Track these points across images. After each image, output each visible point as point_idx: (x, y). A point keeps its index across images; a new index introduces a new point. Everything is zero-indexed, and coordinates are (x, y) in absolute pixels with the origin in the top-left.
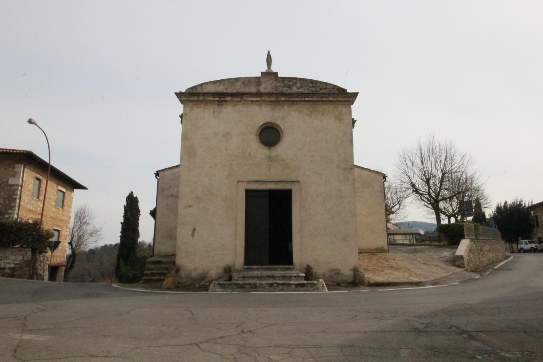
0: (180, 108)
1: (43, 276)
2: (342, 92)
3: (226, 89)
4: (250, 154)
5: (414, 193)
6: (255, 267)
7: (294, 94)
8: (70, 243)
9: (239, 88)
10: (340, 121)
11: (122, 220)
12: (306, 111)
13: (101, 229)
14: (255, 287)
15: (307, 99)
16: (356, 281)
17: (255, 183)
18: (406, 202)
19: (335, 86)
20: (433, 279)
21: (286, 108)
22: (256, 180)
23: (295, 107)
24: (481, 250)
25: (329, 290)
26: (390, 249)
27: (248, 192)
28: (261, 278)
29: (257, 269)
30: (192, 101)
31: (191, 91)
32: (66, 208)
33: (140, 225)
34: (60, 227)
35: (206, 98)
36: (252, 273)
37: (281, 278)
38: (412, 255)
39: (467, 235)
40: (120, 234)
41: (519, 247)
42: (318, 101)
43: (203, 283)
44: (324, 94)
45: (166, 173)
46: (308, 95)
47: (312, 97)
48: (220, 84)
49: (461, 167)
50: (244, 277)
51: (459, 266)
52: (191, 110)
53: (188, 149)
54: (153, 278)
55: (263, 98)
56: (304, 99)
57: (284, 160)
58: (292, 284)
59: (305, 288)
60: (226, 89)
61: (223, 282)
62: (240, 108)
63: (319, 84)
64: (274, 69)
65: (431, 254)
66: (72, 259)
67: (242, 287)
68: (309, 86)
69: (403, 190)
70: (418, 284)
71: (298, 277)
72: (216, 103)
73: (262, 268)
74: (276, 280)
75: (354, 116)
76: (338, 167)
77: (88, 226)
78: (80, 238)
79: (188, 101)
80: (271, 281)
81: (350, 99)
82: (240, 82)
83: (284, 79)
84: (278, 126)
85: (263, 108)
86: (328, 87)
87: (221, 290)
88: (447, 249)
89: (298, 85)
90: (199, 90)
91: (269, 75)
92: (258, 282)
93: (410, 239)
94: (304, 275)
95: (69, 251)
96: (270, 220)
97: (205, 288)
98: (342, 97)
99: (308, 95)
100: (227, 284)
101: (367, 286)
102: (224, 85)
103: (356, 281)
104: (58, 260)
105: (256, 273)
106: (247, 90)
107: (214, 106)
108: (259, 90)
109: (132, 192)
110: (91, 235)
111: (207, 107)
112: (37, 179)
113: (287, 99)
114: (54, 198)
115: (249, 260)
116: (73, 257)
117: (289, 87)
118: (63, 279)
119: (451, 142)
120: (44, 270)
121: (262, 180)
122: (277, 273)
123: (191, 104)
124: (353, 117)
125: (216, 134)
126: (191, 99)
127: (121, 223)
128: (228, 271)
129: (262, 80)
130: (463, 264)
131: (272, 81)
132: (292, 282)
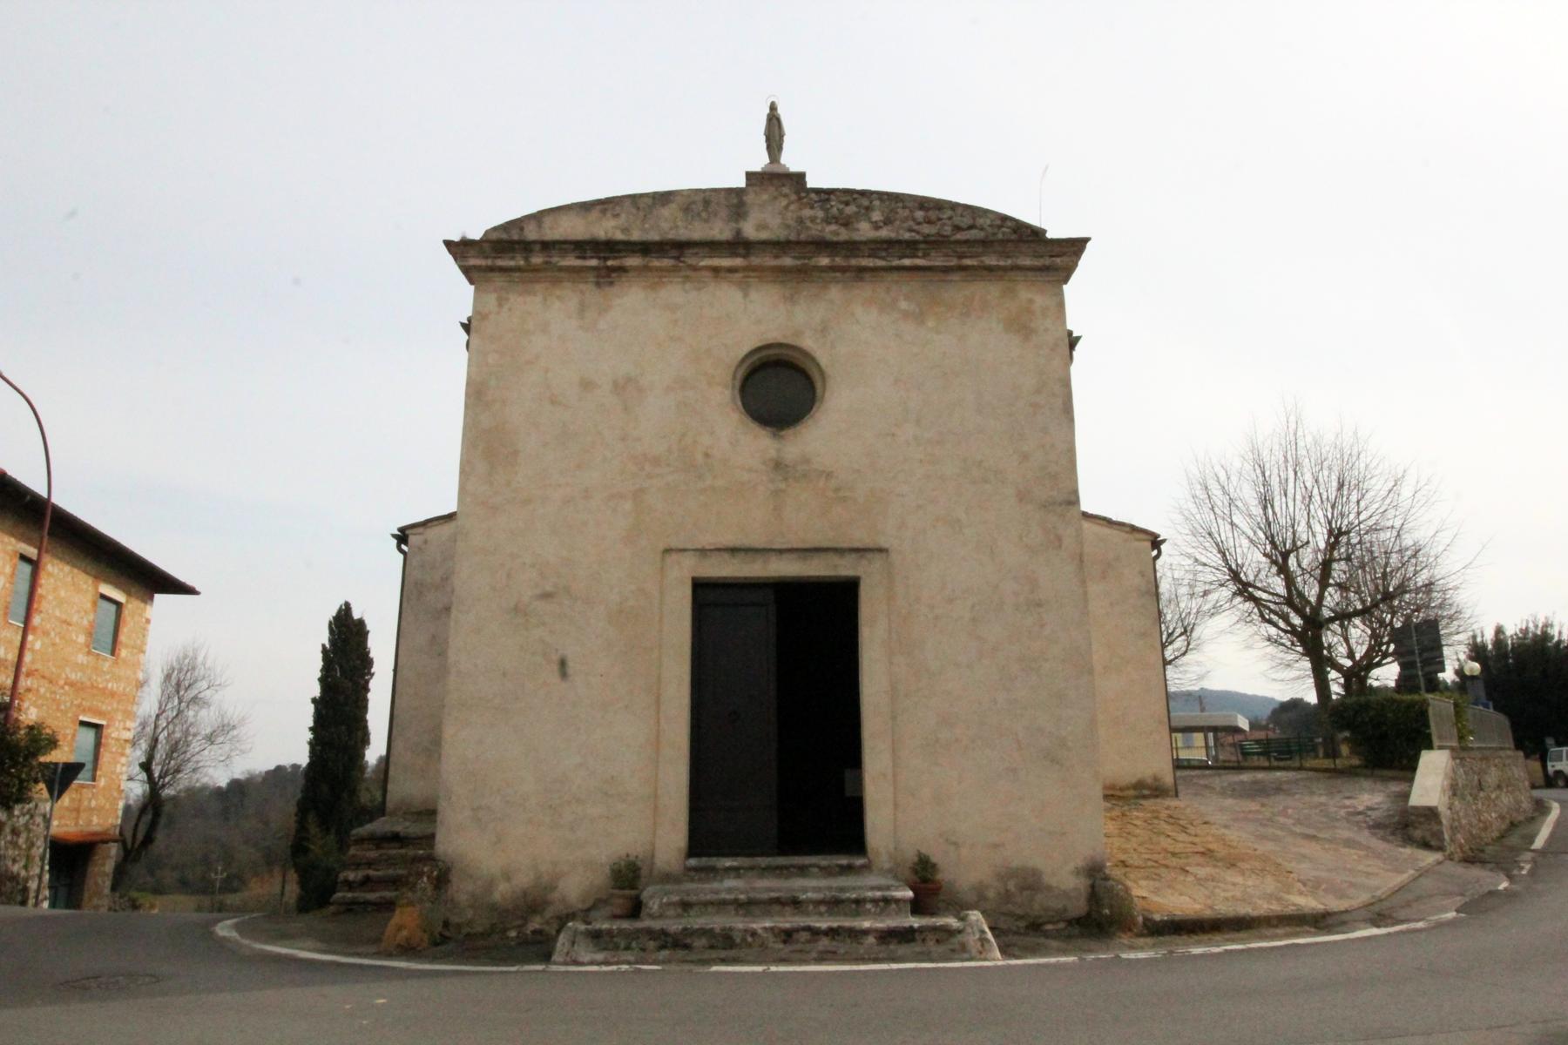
0: (460, 295)
1: (26, 880)
2: (1029, 236)
3: (625, 230)
4: (707, 455)
5: (1239, 599)
6: (728, 862)
7: (861, 242)
8: (146, 767)
9: (669, 225)
10: (1027, 338)
11: (316, 691)
12: (903, 305)
13: (243, 721)
14: (726, 945)
15: (907, 262)
16: (1099, 917)
17: (726, 556)
18: (1206, 630)
19: (1005, 218)
20: (1364, 897)
21: (835, 293)
22: (731, 545)
23: (866, 290)
24: (1481, 787)
25: (1006, 951)
26: (1180, 788)
27: (701, 587)
28: (747, 906)
29: (735, 871)
30: (502, 270)
31: (504, 236)
32: (124, 653)
33: (371, 705)
34: (100, 714)
35: (555, 260)
36: (716, 885)
37: (823, 908)
38: (1253, 806)
39: (1440, 738)
40: (309, 736)
41: (1550, 770)
42: (946, 270)
43: (535, 924)
44: (966, 242)
45: (433, 533)
46: (910, 247)
47: (924, 257)
48: (604, 212)
49: (1391, 513)
50: (686, 906)
51: (1426, 845)
52: (501, 302)
53: (487, 443)
54: (372, 896)
55: (755, 261)
56: (896, 263)
57: (829, 475)
58: (866, 932)
59: (917, 947)
60: (625, 230)
61: (605, 926)
62: (675, 293)
63: (949, 213)
64: (791, 160)
65: (1316, 799)
66: (148, 817)
67: (675, 943)
68: (914, 219)
69: (1199, 589)
70: (1320, 921)
71: (887, 901)
72: (591, 278)
73: (752, 868)
74: (808, 914)
75: (1073, 323)
76: (1022, 497)
77: (203, 713)
78: (174, 748)
79: (491, 269)
80: (788, 921)
81: (1058, 260)
82: (673, 206)
83: (826, 194)
84: (806, 354)
85: (754, 295)
86: (980, 221)
87: (600, 957)
88: (1366, 784)
89: (876, 216)
90: (531, 234)
91: (777, 181)
92: (738, 923)
93: (1207, 747)
94: (910, 894)
95: (137, 789)
96: (781, 686)
97: (540, 948)
98: (1033, 258)
99: (910, 247)
100: (620, 931)
101: (1140, 935)
102: (617, 216)
103: (1099, 917)
104: (95, 820)
105: (731, 886)
106: (697, 231)
107: (582, 286)
108: (738, 232)
109: (347, 605)
110: (210, 739)
111: (558, 292)
112: (24, 558)
113: (839, 261)
114: (85, 622)
115: (707, 836)
116: (153, 804)
117: (846, 223)
118: (108, 883)
119: (1355, 433)
120: (29, 858)
121: (757, 545)
122: (810, 886)
123: (499, 280)
124: (1069, 327)
125: (587, 385)
126: (500, 263)
127: (314, 701)
128: (628, 879)
129: (749, 198)
130: (1438, 835)
131: (784, 202)
132: (867, 924)
